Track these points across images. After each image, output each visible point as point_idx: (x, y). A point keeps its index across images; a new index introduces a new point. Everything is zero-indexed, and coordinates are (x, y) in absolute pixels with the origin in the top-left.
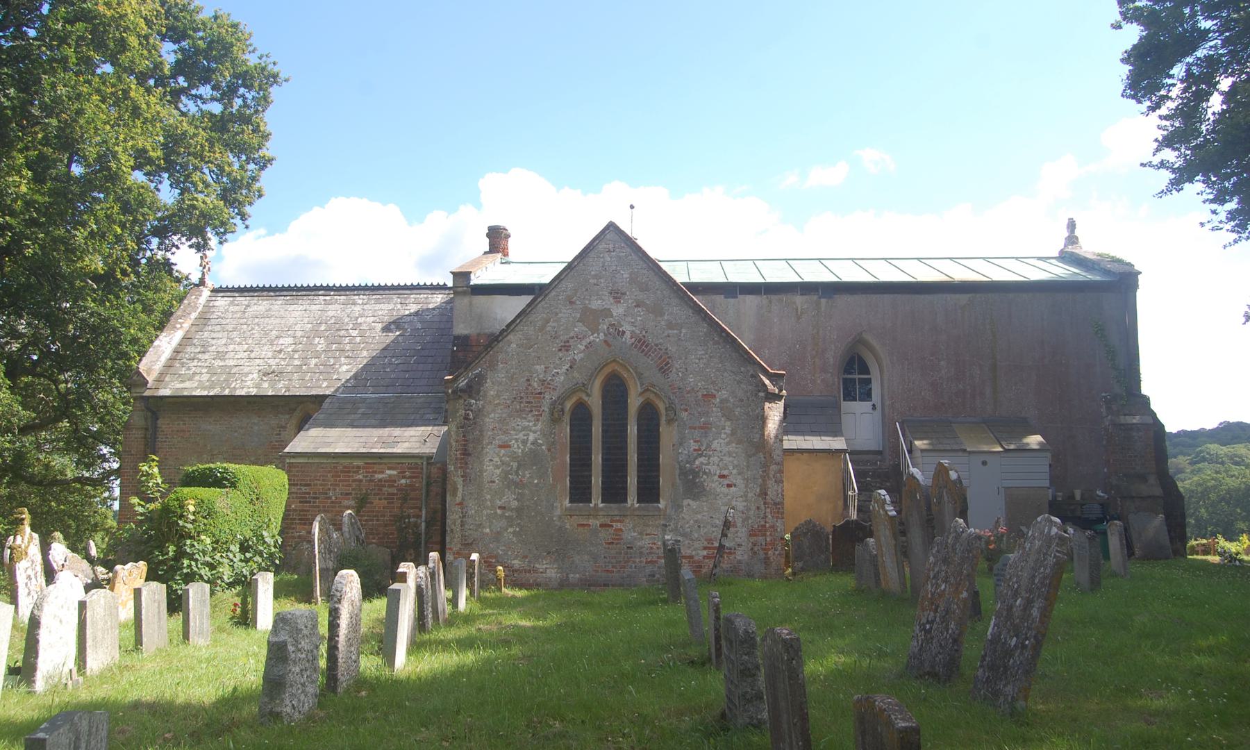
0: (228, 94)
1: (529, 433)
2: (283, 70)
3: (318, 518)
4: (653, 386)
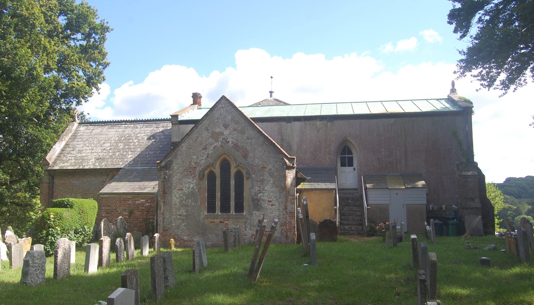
0: (87, 37)
1: (190, 184)
2: (110, 25)
3: (104, 220)
4: (241, 164)
